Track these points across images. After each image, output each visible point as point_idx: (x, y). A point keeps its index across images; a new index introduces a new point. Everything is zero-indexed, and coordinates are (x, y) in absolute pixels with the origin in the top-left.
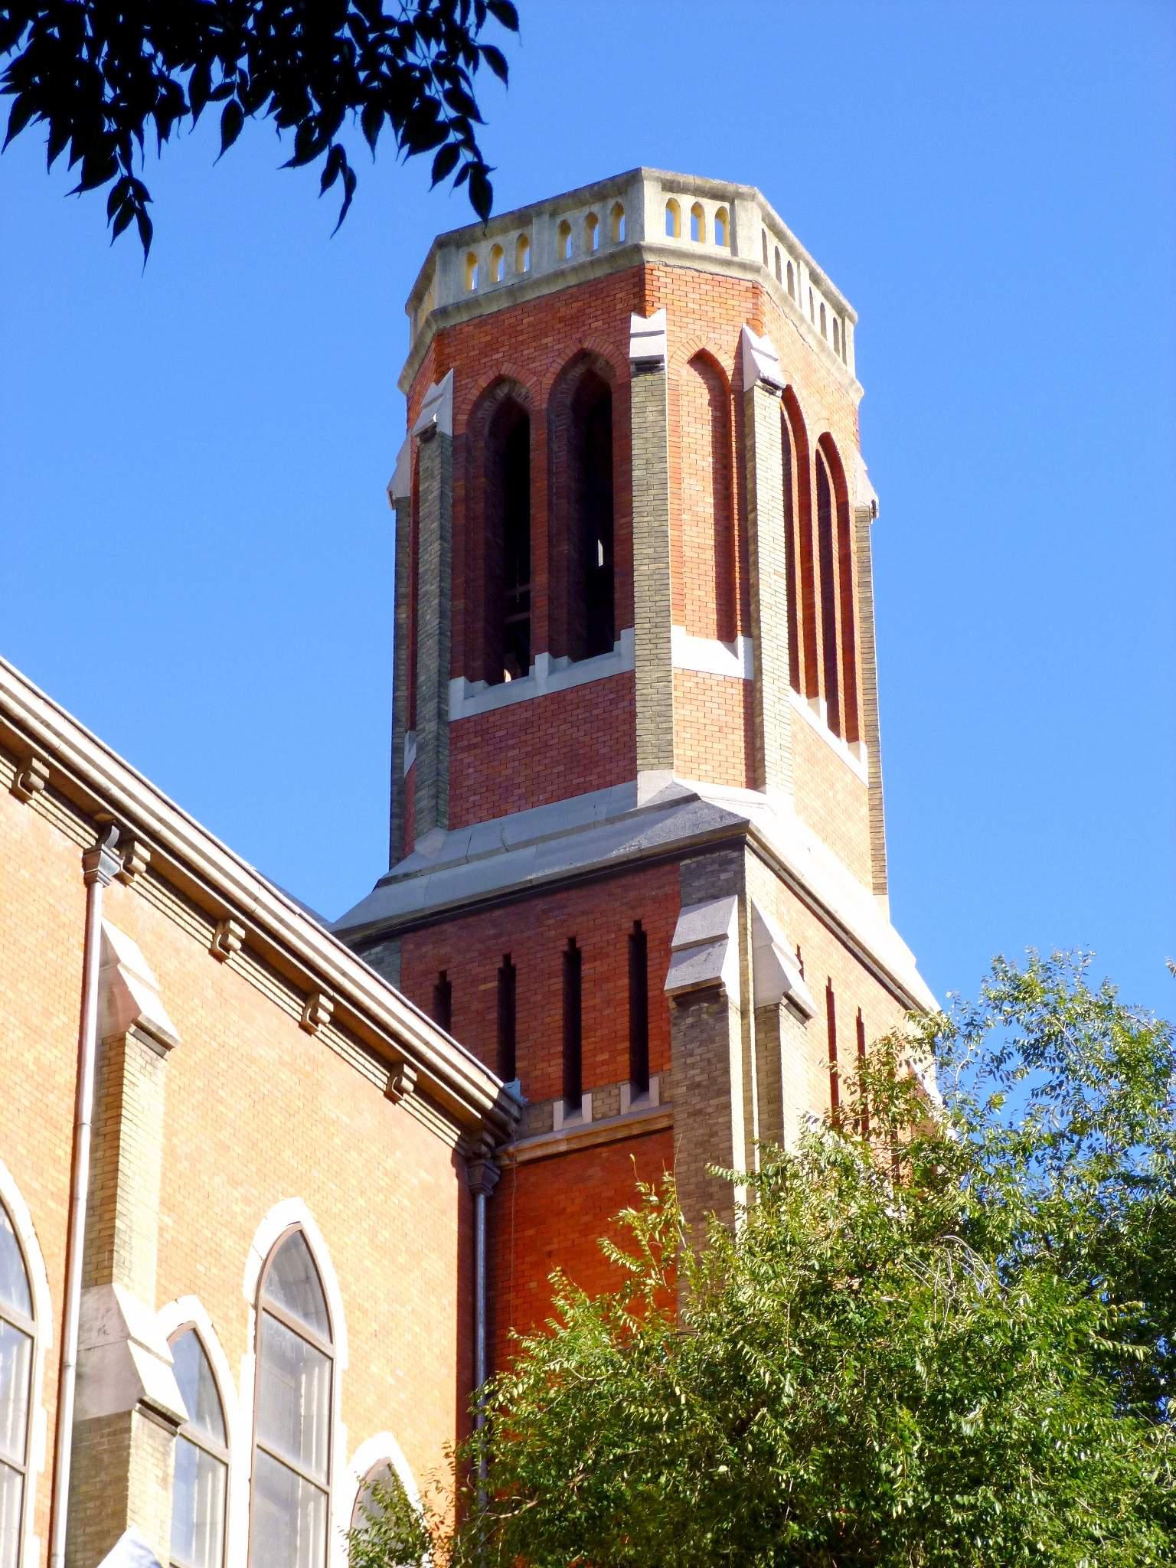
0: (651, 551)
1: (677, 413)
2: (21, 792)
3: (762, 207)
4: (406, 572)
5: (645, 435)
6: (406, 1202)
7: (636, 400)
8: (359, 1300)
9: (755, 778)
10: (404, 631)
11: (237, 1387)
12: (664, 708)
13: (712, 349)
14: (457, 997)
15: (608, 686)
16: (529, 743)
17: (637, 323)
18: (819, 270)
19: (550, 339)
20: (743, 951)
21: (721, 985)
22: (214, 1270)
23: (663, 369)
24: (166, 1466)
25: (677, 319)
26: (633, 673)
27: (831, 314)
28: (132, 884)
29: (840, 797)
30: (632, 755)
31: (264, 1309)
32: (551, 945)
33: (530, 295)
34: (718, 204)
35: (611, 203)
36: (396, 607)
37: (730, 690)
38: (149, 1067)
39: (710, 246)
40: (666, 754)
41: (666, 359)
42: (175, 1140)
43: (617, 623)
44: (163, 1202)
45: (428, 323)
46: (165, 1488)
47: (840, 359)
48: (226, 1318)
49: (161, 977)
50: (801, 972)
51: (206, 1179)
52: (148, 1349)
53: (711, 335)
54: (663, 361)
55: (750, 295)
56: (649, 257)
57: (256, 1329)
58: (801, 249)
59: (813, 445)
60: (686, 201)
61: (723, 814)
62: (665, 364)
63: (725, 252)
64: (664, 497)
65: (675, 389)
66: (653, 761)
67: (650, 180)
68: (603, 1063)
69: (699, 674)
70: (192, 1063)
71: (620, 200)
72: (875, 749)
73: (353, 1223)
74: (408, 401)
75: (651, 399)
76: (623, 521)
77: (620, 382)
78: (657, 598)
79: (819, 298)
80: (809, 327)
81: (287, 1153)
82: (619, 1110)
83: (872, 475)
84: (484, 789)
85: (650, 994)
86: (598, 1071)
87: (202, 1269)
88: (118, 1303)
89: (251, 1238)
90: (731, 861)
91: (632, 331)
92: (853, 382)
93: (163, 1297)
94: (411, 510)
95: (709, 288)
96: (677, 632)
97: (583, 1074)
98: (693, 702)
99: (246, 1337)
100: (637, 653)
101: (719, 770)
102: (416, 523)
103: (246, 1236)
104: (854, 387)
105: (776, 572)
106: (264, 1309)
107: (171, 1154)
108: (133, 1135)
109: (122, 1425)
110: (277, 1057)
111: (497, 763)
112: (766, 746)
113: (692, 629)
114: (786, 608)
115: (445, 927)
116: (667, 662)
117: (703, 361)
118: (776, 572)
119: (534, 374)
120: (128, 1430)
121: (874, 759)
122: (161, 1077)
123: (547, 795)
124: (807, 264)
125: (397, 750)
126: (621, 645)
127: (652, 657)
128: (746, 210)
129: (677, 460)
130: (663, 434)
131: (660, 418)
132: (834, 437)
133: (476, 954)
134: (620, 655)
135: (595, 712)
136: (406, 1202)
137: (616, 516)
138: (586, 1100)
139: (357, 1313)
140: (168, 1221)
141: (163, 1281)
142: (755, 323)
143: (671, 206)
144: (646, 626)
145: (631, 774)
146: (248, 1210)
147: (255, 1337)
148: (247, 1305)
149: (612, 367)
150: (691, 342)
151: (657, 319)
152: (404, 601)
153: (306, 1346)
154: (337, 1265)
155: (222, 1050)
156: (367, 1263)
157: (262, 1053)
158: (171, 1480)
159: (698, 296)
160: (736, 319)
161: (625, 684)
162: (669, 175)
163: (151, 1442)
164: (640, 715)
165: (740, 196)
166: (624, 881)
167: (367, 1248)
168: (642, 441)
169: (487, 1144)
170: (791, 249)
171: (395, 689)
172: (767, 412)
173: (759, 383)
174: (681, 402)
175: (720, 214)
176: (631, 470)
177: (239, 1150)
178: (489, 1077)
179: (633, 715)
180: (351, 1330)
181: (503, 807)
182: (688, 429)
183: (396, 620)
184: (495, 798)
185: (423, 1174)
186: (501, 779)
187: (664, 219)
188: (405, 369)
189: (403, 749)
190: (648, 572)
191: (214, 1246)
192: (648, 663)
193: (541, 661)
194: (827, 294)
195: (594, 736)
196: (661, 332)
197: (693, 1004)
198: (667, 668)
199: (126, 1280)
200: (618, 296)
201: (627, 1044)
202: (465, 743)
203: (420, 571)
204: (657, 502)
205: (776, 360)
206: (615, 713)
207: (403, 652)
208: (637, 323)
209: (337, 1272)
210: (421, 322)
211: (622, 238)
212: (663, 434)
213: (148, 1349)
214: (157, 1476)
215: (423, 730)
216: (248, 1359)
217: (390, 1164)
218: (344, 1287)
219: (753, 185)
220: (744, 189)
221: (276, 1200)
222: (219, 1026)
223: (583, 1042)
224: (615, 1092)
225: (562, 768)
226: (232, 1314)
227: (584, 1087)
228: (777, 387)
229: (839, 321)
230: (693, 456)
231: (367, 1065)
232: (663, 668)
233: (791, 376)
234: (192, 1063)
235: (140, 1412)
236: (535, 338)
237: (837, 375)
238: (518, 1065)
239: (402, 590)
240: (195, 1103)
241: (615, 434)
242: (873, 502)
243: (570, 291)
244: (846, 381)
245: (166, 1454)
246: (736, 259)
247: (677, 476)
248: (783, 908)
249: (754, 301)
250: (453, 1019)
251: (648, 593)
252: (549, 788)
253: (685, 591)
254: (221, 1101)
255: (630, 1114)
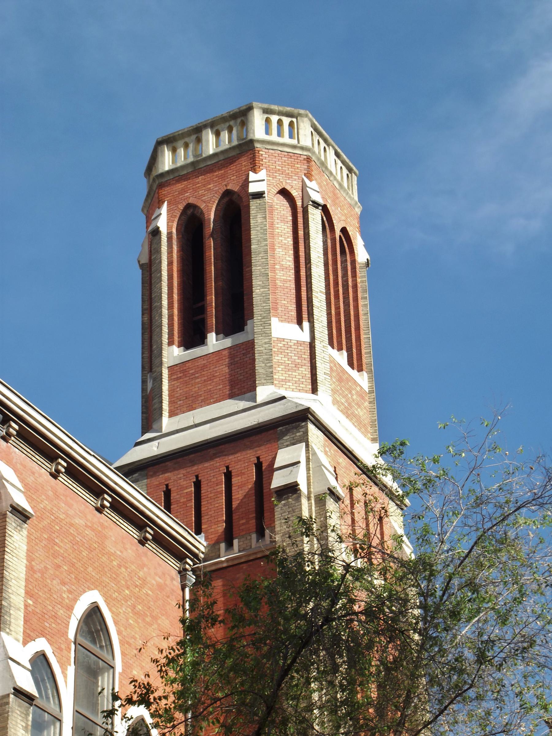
0: (261, 283)
1: (272, 218)
2: (143, 542)
3: (311, 120)
4: (146, 298)
5: (257, 229)
6: (150, 592)
7: (252, 212)
8: (127, 639)
9: (314, 390)
10: (147, 326)
11: (66, 682)
12: (268, 356)
13: (288, 188)
14: (174, 496)
15: (242, 347)
16: (205, 375)
17: (252, 176)
18: (339, 150)
19: (212, 185)
20: (308, 469)
21: (298, 485)
22: (53, 625)
23: (265, 197)
24: (27, 720)
25: (271, 174)
26: (254, 340)
27: (345, 171)
28: (10, 441)
29: (355, 397)
30: (253, 379)
31: (79, 644)
32: (217, 470)
33: (202, 165)
34: (290, 119)
35: (239, 120)
36: (143, 314)
37: (300, 347)
38: (19, 528)
39: (286, 139)
40: (270, 378)
41: (266, 193)
42: (33, 563)
43: (245, 317)
44: (27, 593)
45: (154, 180)
46: (26, 731)
47: (350, 192)
48: (60, 649)
49: (26, 485)
50: (336, 478)
51: (50, 582)
52: (18, 664)
53: (288, 181)
54: (264, 193)
55: (306, 162)
56: (257, 145)
57: (75, 654)
58: (330, 140)
59: (338, 233)
60: (274, 118)
61: (297, 405)
62: (266, 195)
63: (294, 142)
64: (266, 257)
65: (271, 206)
66: (263, 381)
67: (257, 108)
68: (243, 524)
69: (285, 340)
70: (42, 526)
71: (243, 118)
72: (371, 375)
73: (123, 602)
74: (146, 218)
75: (260, 211)
76: (247, 270)
77: (245, 204)
78: (264, 305)
79: (340, 164)
80: (335, 177)
81: (90, 569)
82: (251, 546)
83: (367, 247)
84: (185, 398)
85: (264, 491)
86: (241, 528)
87: (48, 625)
88: (3, 642)
89: (73, 610)
90: (302, 427)
91: (250, 180)
92: (356, 203)
93: (28, 639)
94: (148, 269)
95: (286, 159)
96: (274, 321)
97: (234, 530)
98: (283, 353)
99: (70, 657)
100: (255, 331)
101: (296, 385)
102: (151, 275)
103: (70, 609)
104: (357, 206)
105: (321, 292)
106: (79, 644)
107: (30, 569)
108: (11, 560)
109: (5, 700)
110: (84, 524)
111: (191, 385)
112: (317, 373)
113: (281, 319)
114: (326, 308)
115: (167, 463)
116: (270, 335)
117: (284, 193)
118: (321, 292)
119: (205, 202)
120: (8, 703)
121: (371, 380)
122: (25, 533)
123: (215, 400)
124: (333, 147)
125: (144, 382)
126: (248, 328)
127: (262, 332)
128: (303, 122)
129: (273, 240)
130: (265, 228)
131: (264, 220)
132: (348, 229)
133: (182, 475)
134: (247, 332)
135: (236, 360)
136: (150, 592)
137: (244, 267)
138: (236, 542)
139: (126, 645)
140: (30, 602)
141: (28, 631)
142: (309, 175)
143: (268, 121)
144: (259, 318)
145: (253, 388)
146: (70, 596)
147: (75, 658)
148: (70, 643)
149: (241, 198)
150: (278, 185)
151: (262, 174)
152: (146, 312)
153: (101, 662)
154: (116, 623)
155: (57, 520)
156: (131, 621)
157: (77, 522)
158: (30, 728)
159: (280, 163)
160: (299, 173)
161: (250, 346)
162: (265, 106)
163: (19, 709)
164: (257, 360)
165: (300, 115)
166: (251, 439)
167: (131, 614)
168: (256, 232)
169: (190, 565)
170: (325, 141)
171: (143, 353)
172: (315, 216)
173: (311, 203)
174: (274, 213)
175: (291, 124)
176: (251, 245)
177: (66, 568)
178: (189, 533)
179: (254, 360)
180: (123, 654)
181: (194, 406)
182: (277, 226)
183: (142, 321)
184: (190, 402)
185: (158, 579)
186: (192, 393)
187: (264, 127)
188: (144, 203)
189: (147, 381)
190: (260, 293)
191: (53, 614)
192: (260, 335)
193: (212, 337)
194: (343, 162)
195: (236, 371)
196: (263, 180)
197: (285, 495)
198: (270, 337)
199: (8, 630)
200: (243, 164)
201: (254, 515)
202: (176, 377)
203: (153, 296)
204: (264, 260)
205: (318, 192)
206: (246, 360)
207: (146, 336)
208: (252, 176)
209: (115, 626)
210: (151, 180)
211: (245, 137)
212: (265, 228)
213: (18, 664)
214: (22, 726)
215: (155, 371)
216: (71, 670)
217: (141, 574)
218: (119, 633)
219: (306, 109)
220: (302, 111)
221: (85, 592)
222: (55, 509)
223: (234, 515)
224: (249, 538)
225: (221, 386)
226: (63, 647)
227: (234, 536)
228: (319, 205)
229: (350, 175)
230: (280, 238)
231: (32, 453)
232: (268, 337)
233: (327, 200)
234: (42, 526)
235: (14, 694)
236: (204, 186)
237: (349, 200)
238: (203, 527)
239: (145, 307)
240: (43, 545)
241: (243, 229)
242: (367, 260)
243: (220, 163)
244: (353, 203)
245: (27, 715)
246: (299, 145)
247: (273, 247)
248: (327, 449)
249: (308, 164)
250: (172, 507)
251: (260, 303)
252: (215, 396)
253: (278, 301)
254: (56, 544)
255: (256, 548)
